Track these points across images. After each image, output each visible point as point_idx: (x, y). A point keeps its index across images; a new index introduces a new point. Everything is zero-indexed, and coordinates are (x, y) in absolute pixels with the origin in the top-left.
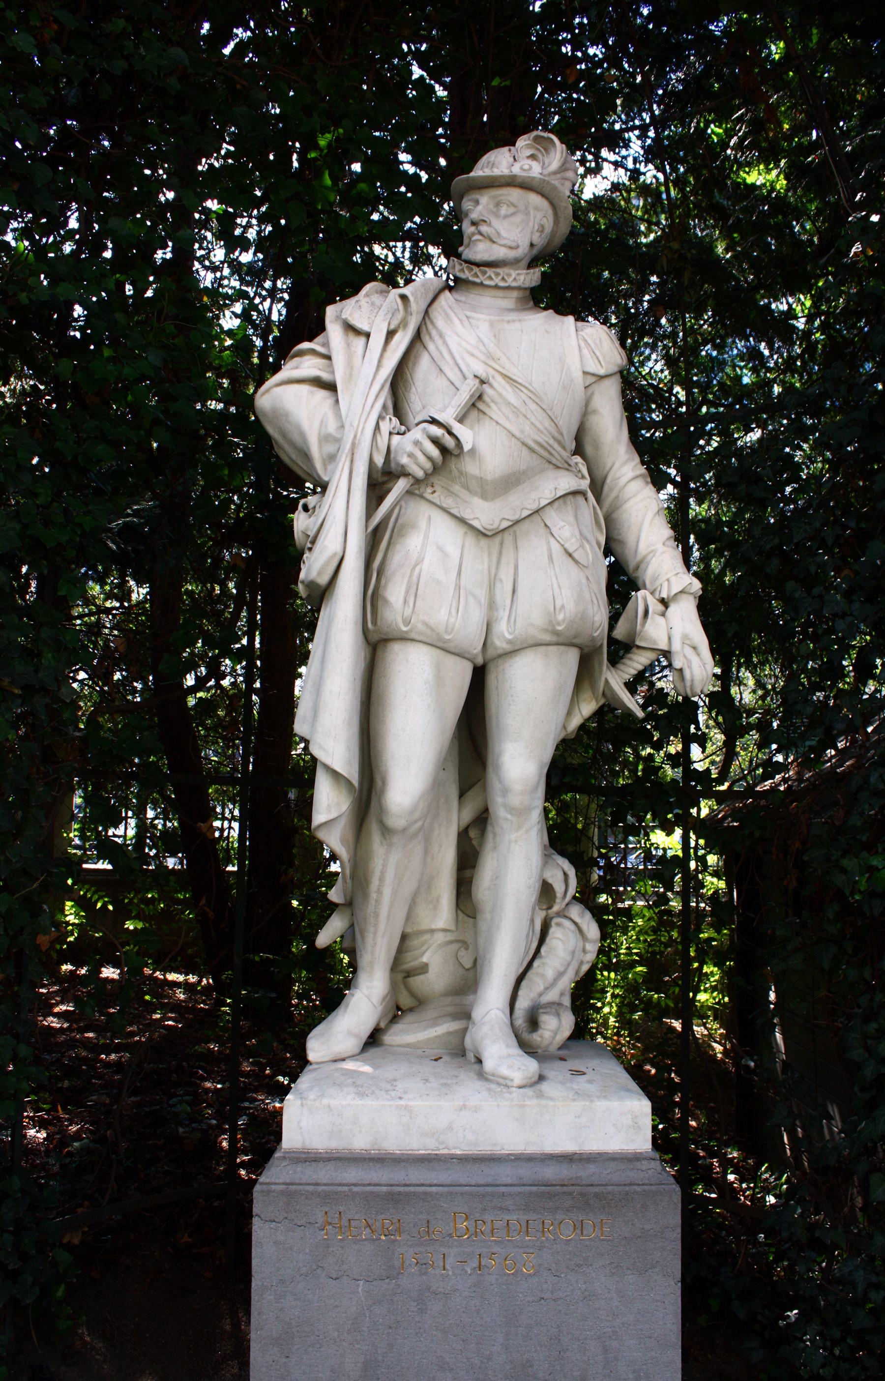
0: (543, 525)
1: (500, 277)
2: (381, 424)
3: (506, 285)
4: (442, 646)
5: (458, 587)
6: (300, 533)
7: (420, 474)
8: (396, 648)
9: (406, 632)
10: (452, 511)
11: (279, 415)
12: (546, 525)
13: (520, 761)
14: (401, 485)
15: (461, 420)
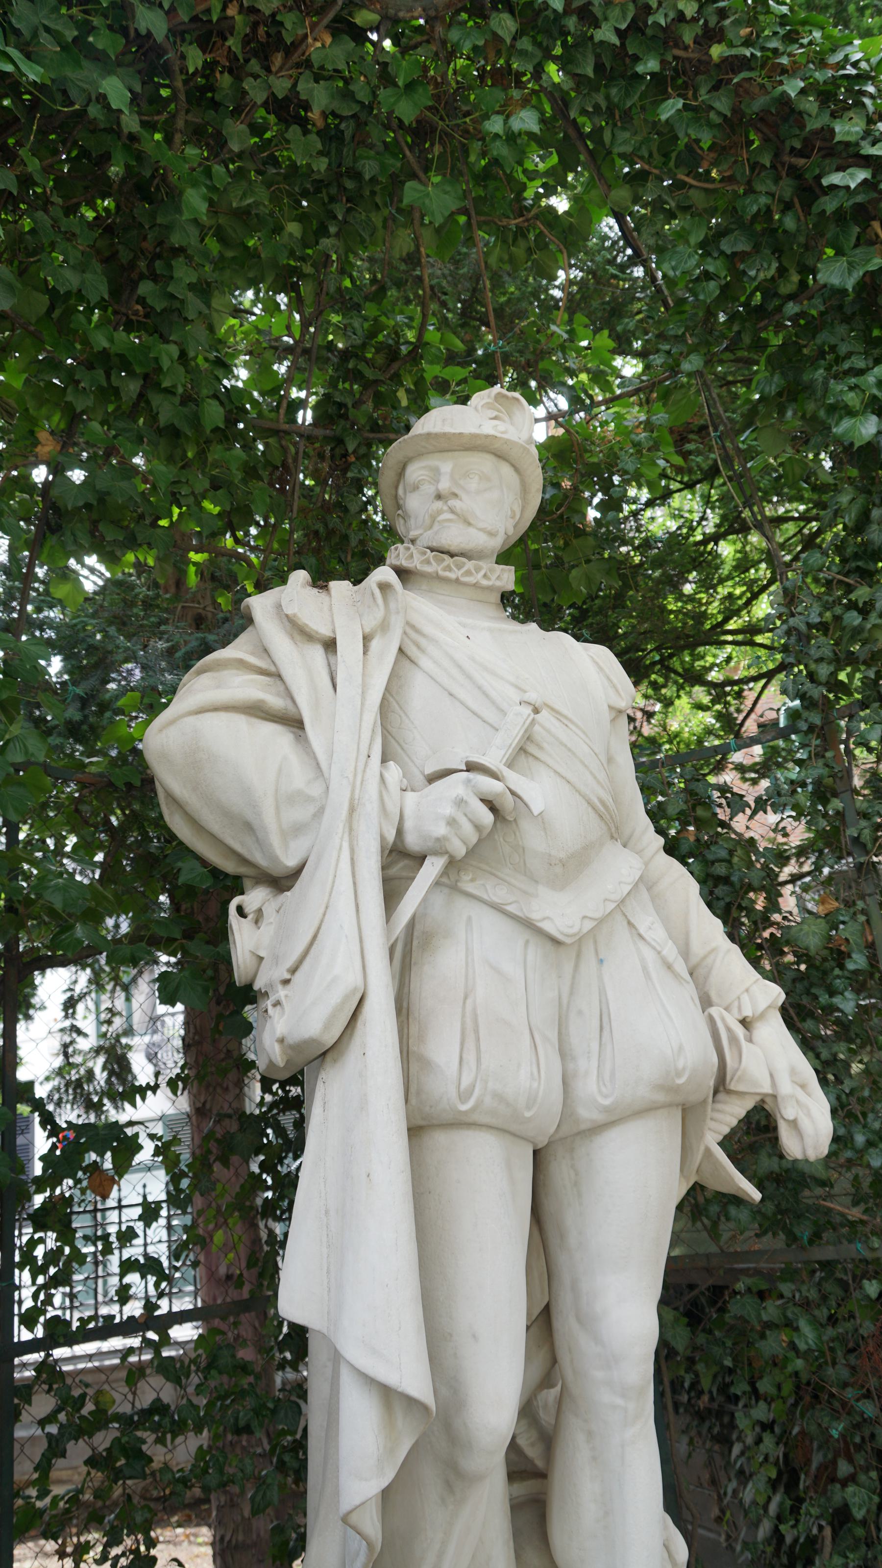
0: (625, 923)
1: (482, 573)
2: (387, 775)
3: (490, 583)
6: (248, 956)
7: (460, 851)
9: (466, 1113)
10: (509, 908)
12: (629, 923)
14: (431, 869)
15: (510, 765)
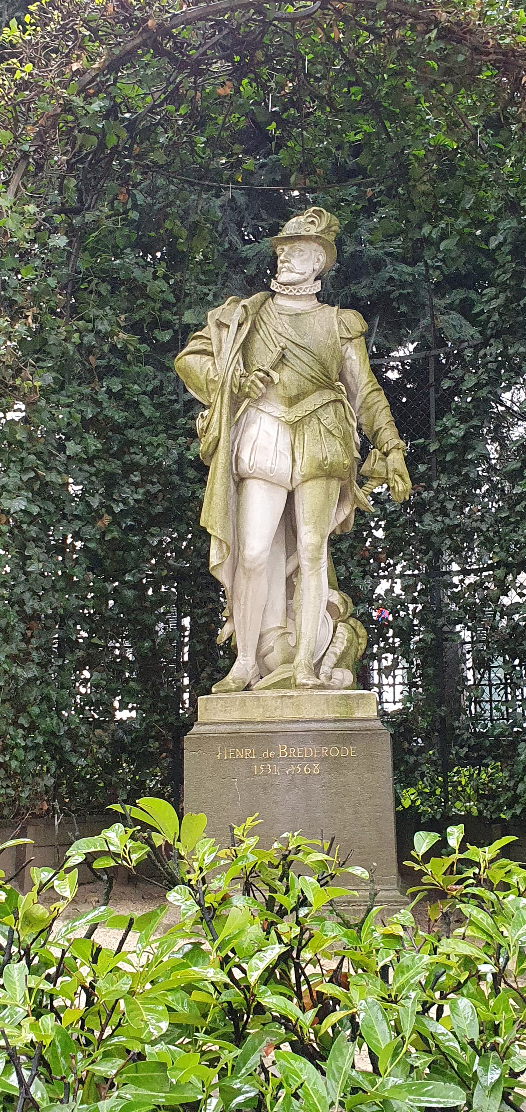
4: (267, 480)
5: (276, 450)
8: (248, 482)
11: (188, 371)
13: (311, 537)
15: (273, 368)
